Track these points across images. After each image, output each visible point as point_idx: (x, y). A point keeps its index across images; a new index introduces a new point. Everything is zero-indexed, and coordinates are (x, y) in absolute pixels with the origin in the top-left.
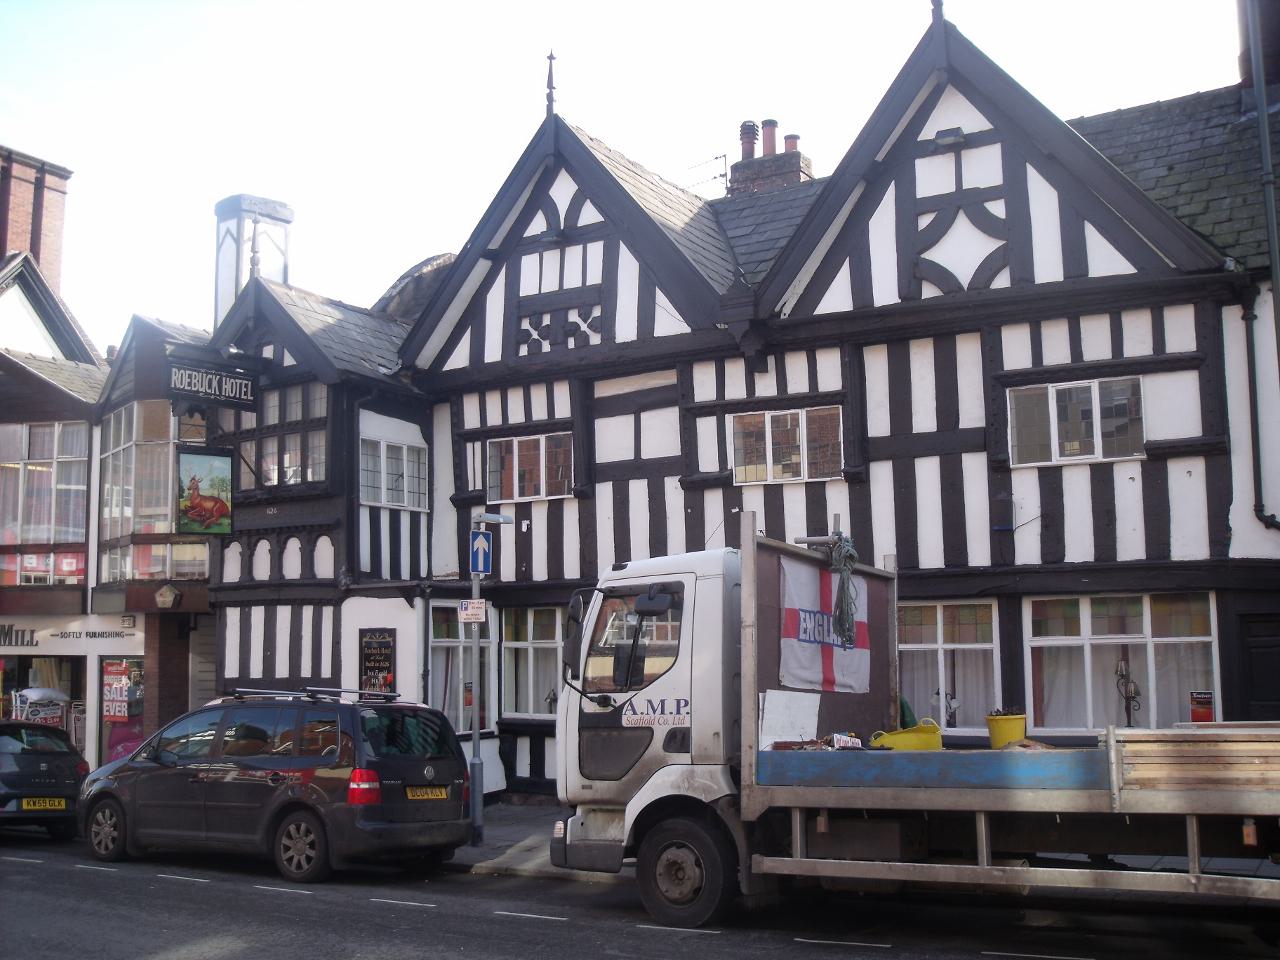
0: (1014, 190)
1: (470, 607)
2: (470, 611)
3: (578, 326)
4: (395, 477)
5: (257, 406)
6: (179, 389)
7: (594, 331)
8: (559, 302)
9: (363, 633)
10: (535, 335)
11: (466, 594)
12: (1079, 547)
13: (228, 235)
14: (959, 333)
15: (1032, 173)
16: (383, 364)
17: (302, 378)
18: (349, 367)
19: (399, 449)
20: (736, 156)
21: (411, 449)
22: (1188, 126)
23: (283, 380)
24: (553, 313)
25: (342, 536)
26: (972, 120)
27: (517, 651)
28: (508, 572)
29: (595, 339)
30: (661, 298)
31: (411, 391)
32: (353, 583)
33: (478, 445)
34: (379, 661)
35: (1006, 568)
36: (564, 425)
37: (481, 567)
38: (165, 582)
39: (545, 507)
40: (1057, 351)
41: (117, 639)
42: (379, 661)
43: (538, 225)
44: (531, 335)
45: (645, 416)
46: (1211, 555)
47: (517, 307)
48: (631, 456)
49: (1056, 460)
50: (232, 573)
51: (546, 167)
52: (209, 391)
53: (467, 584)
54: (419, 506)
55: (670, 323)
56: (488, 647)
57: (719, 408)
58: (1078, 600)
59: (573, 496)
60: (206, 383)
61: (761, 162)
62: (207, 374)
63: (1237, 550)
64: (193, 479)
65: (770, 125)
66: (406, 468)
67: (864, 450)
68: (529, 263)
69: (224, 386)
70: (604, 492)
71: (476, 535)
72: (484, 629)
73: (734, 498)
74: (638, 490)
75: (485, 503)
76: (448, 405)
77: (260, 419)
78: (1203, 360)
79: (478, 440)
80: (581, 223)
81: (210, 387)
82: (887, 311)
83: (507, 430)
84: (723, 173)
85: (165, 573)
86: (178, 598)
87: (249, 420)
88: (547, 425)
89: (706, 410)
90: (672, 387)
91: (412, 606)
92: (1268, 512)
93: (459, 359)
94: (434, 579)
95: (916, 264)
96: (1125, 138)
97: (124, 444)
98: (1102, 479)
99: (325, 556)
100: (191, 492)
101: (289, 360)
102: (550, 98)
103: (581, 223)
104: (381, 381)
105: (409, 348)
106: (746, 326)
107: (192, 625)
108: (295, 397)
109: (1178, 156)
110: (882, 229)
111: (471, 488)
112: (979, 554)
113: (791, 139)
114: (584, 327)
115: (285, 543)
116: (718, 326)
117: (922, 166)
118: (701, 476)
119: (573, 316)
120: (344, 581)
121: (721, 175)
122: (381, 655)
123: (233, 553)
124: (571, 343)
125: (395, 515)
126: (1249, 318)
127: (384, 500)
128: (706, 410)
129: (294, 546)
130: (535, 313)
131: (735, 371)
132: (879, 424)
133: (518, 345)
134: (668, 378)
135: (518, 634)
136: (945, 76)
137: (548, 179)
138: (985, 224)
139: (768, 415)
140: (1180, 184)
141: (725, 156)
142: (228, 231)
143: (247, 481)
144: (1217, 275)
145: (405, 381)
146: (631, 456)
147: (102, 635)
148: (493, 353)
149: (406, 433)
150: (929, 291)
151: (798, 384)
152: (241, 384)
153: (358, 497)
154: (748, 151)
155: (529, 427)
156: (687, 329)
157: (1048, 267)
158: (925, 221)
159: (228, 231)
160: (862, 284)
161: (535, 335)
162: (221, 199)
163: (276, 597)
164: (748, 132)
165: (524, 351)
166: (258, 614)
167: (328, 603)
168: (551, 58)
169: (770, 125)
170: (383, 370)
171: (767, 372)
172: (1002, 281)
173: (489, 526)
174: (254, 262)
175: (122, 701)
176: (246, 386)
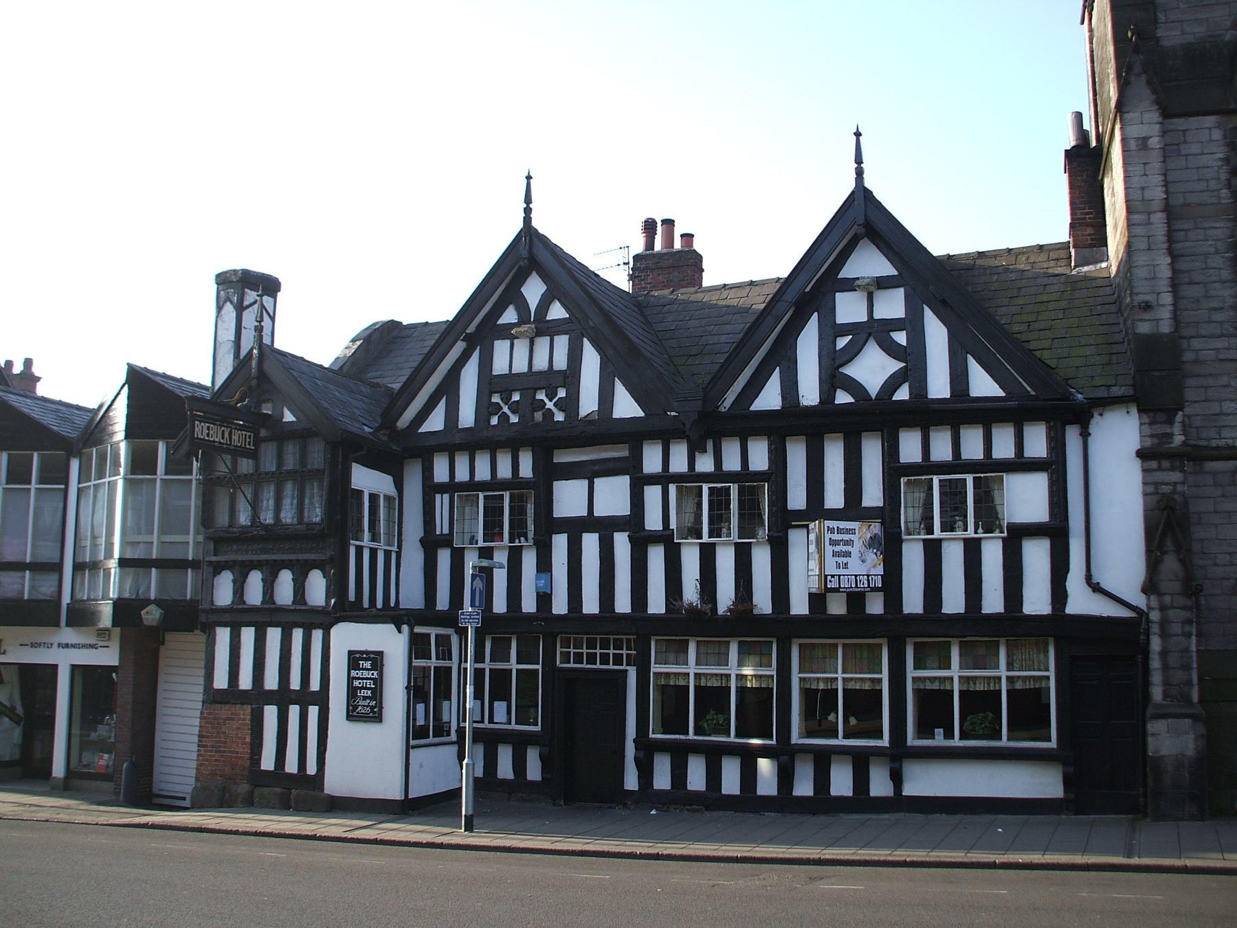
0: (913, 324)
5: (254, 455)
12: (953, 601)
20: (638, 247)
24: (523, 391)
26: (879, 265)
29: (559, 417)
33: (446, 497)
43: (510, 316)
47: (489, 383)
49: (937, 533)
52: (222, 441)
55: (626, 406)
57: (664, 479)
58: (688, 640)
60: (220, 435)
61: (659, 255)
62: (221, 426)
63: (1073, 607)
65: (669, 223)
67: (785, 521)
68: (501, 349)
69: (233, 437)
70: (560, 543)
74: (590, 543)
76: (420, 459)
79: (446, 493)
84: (627, 261)
87: (245, 466)
88: (529, 482)
89: (653, 479)
91: (400, 632)
92: (1095, 581)
93: (435, 422)
95: (834, 376)
97: (95, 480)
98: (973, 551)
99: (317, 589)
101: (289, 417)
102: (528, 211)
111: (438, 532)
113: (688, 237)
116: (669, 413)
118: (647, 533)
119: (541, 396)
121: (624, 264)
125: (374, 552)
128: (653, 479)
132: (797, 498)
134: (621, 452)
138: (891, 349)
140: (1109, 386)
141: (628, 247)
147: (73, 646)
150: (843, 398)
152: (246, 435)
154: (650, 244)
156: (642, 414)
157: (939, 386)
158: (842, 342)
160: (790, 387)
162: (282, 284)
165: (494, 421)
166: (248, 635)
169: (669, 223)
171: (706, 452)
172: (903, 394)
176: (250, 438)
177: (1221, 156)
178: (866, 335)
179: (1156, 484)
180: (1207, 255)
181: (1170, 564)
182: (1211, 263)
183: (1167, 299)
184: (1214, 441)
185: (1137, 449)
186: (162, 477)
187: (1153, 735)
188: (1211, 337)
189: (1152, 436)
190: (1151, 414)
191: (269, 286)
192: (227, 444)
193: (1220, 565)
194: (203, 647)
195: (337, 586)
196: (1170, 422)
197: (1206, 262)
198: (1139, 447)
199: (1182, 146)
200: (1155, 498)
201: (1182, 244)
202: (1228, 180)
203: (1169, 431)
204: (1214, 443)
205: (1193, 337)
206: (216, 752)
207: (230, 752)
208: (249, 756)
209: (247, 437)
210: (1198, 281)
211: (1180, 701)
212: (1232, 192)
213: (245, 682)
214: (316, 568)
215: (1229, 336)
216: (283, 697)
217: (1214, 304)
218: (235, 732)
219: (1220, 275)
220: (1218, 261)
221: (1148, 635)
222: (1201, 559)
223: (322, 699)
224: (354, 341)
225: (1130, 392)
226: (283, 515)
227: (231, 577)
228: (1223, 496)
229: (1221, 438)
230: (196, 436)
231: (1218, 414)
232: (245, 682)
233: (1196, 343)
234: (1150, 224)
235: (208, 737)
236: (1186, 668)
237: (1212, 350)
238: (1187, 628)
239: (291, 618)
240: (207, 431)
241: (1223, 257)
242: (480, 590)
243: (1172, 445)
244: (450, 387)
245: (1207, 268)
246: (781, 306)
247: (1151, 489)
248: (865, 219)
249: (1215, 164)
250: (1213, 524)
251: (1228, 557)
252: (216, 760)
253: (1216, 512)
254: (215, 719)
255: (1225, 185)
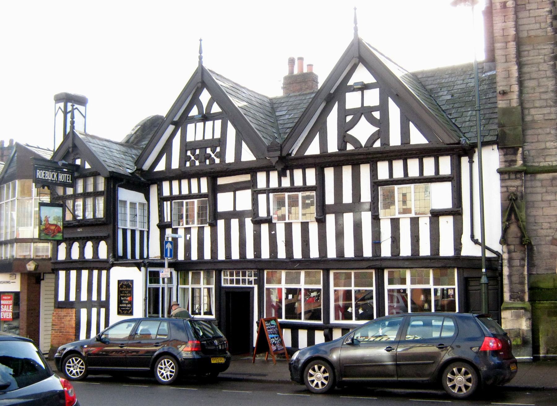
0: (383, 108)
1: (164, 272)
2: (164, 273)
3: (211, 156)
4: (133, 216)
5: (73, 185)
6: (40, 179)
7: (217, 158)
8: (203, 145)
9: (119, 282)
10: (193, 158)
11: (162, 265)
13: (60, 110)
14: (361, 164)
15: (390, 100)
16: (129, 169)
17: (95, 174)
18: (114, 170)
19: (135, 204)
20: (286, 73)
21: (140, 203)
22: (463, 77)
23: (85, 175)
24: (200, 149)
25: (110, 241)
26: (369, 79)
27: (184, 289)
28: (181, 257)
29: (217, 161)
30: (244, 145)
31: (140, 179)
32: (116, 261)
34: (126, 293)
35: (378, 258)
36: (205, 196)
37: (169, 255)
38: (30, 260)
39: (197, 229)
40: (398, 173)
41: (8, 284)
42: (126, 293)
43: (194, 112)
44: (191, 158)
45: (237, 193)
46: (454, 254)
47: (186, 146)
48: (232, 209)
50: (62, 256)
51: (198, 87)
52: (53, 179)
53: (164, 261)
54: (144, 228)
55: (248, 156)
56: (172, 288)
57: (267, 191)
59: (208, 225)
60: (51, 176)
62: (52, 172)
63: (465, 252)
64: (46, 217)
65: (301, 59)
66: (138, 212)
68: (190, 127)
69: (59, 177)
70: (221, 224)
71: (167, 242)
72: (170, 280)
73: (272, 227)
74: (235, 223)
75: (171, 227)
77: (75, 191)
78: (453, 178)
79: (169, 201)
80: (212, 112)
81: (53, 177)
82: (333, 155)
83: (181, 197)
85: (31, 255)
86: (37, 267)
87: (70, 191)
88: (197, 195)
89: (262, 191)
90: (249, 181)
93: (161, 167)
94: (150, 258)
96: (438, 81)
97: (6, 200)
100: (45, 222)
101: (88, 166)
102: (200, 58)
103: (212, 112)
104: (127, 176)
105: (139, 161)
106: (277, 159)
107: (42, 278)
108: (91, 181)
109: (456, 91)
110: (332, 119)
111: (166, 221)
112: (368, 252)
113: (310, 66)
114: (213, 156)
115: (86, 243)
116: (267, 158)
117: (348, 95)
119: (209, 151)
120: (111, 260)
122: (127, 291)
123: (62, 248)
124: (208, 162)
125: (133, 232)
126: (471, 162)
127: (129, 226)
128: (262, 191)
129: (89, 245)
130: (193, 149)
131: (274, 175)
132: (330, 199)
133: (186, 162)
134: (247, 178)
135: (185, 282)
136: (357, 60)
137: (198, 92)
138: (372, 121)
139: (287, 194)
142: (60, 108)
143: (69, 217)
144: (457, 145)
145: (137, 175)
146: (232, 209)
148: (175, 165)
149: (137, 197)
150: (350, 147)
151: (298, 182)
152: (66, 176)
153: (118, 225)
155: (190, 196)
156: (254, 159)
157: (395, 140)
158: (349, 118)
159: (60, 108)
160: (323, 143)
161: (193, 158)
163: (82, 266)
164: (292, 62)
165: (188, 164)
167: (104, 269)
168: (201, 40)
169: (301, 59)
170: (130, 171)
171: (286, 176)
172: (377, 144)
173: (173, 239)
174: (73, 123)
175: (9, 312)
176: (69, 177)
177: (548, 9)
178: (361, 114)
179: (507, 187)
180: (539, 63)
181: (513, 228)
182: (541, 67)
183: (516, 88)
184: (542, 163)
185: (497, 168)
186: (35, 198)
187: (504, 318)
188: (541, 107)
189: (505, 161)
190: (505, 150)
191: (82, 101)
192: (55, 181)
193: (544, 229)
194: (54, 281)
195: (113, 248)
196: (515, 153)
197: (538, 68)
198: (499, 167)
199: (527, 5)
200: (507, 194)
201: (527, 58)
202: (552, 22)
203: (514, 159)
204: (542, 164)
205: (532, 108)
206: (60, 332)
207: (66, 332)
208: (74, 334)
209: (68, 177)
210: (534, 78)
211: (518, 301)
212: (553, 29)
213: (72, 298)
214: (103, 240)
215: (551, 106)
216: (89, 305)
217: (543, 90)
218: (68, 323)
219: (546, 74)
220: (544, 67)
221: (502, 266)
222: (534, 226)
223: (106, 305)
224: (137, 126)
225: (494, 138)
226: (87, 214)
227: (65, 246)
228: (546, 192)
229: (545, 161)
230: (37, 177)
231: (544, 149)
232: (72, 298)
233: (533, 111)
234: (506, 48)
235: (56, 325)
236: (522, 283)
237: (541, 114)
238: (522, 262)
239: (92, 265)
240: (44, 175)
241: (548, 64)
242: (170, 249)
243: (516, 166)
244: (167, 148)
245: (539, 70)
246: (319, 100)
247: (505, 189)
248: (359, 54)
249: (544, 14)
250: (540, 207)
251: (549, 225)
252: (60, 337)
253: (542, 201)
254: (59, 316)
255: (549, 26)
